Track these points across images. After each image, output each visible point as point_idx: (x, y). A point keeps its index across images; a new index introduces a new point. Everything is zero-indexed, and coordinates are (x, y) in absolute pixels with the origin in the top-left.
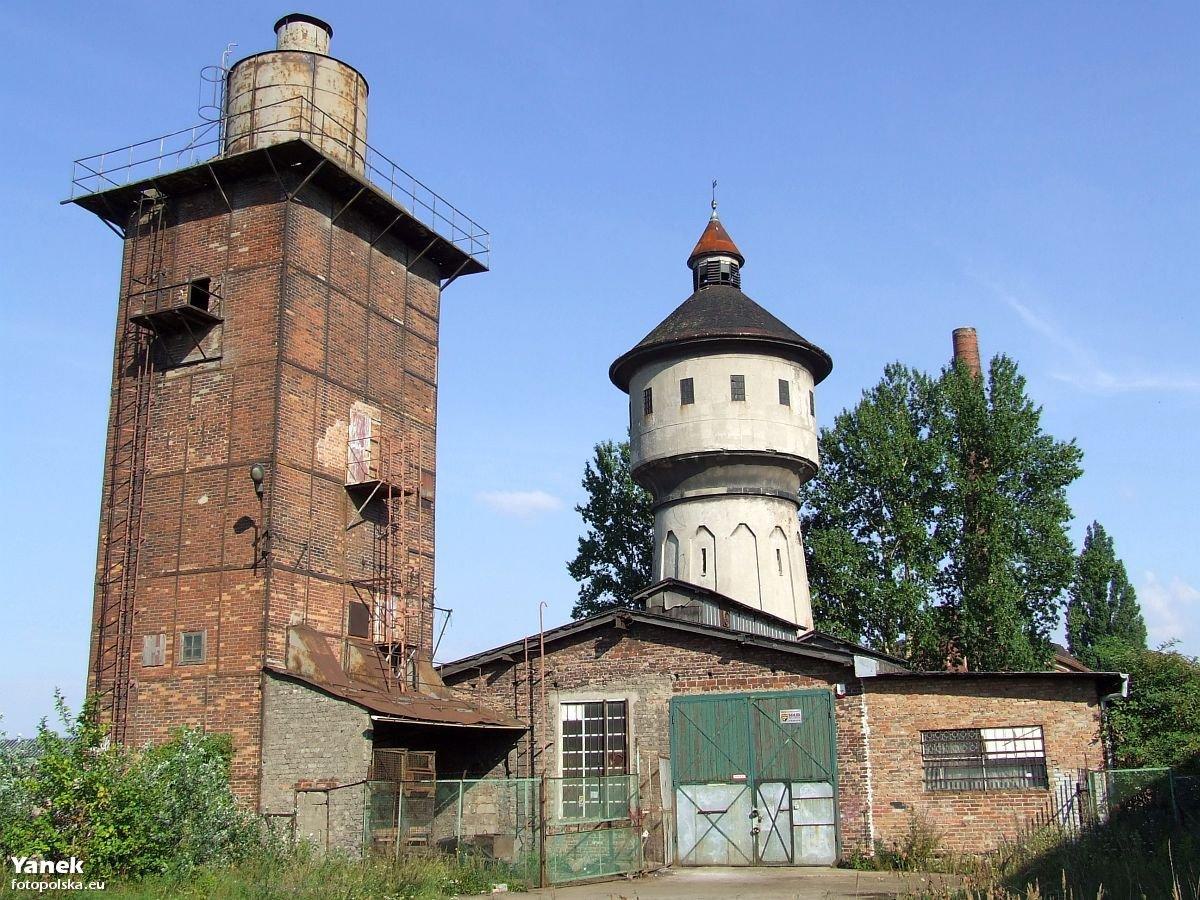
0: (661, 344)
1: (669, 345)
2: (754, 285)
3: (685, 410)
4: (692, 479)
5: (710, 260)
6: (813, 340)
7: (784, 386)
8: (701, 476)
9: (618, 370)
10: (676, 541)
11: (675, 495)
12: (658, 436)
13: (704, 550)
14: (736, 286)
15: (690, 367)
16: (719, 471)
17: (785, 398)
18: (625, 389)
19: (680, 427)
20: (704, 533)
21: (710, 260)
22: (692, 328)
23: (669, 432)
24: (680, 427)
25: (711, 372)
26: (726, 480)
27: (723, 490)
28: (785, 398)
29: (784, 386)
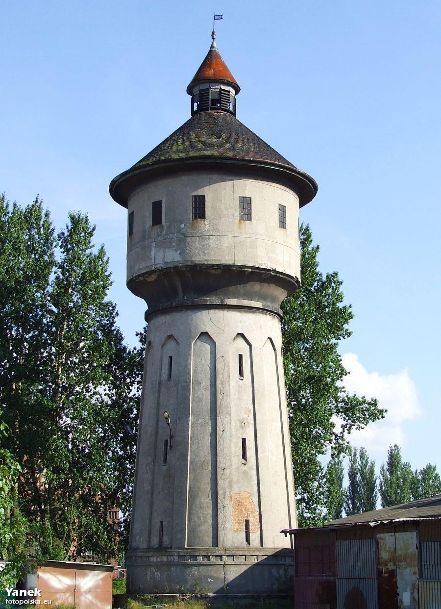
0: (235, 159)
1: (213, 161)
2: (253, 113)
3: (243, 225)
4: (232, 288)
5: (223, 87)
6: (301, 167)
7: (282, 210)
8: (241, 288)
9: (118, 185)
10: (213, 343)
11: (201, 300)
12: (213, 242)
13: (171, 358)
14: (234, 114)
15: (250, 187)
16: (257, 287)
17: (283, 223)
18: (124, 204)
19: (239, 239)
20: (241, 341)
21: (223, 87)
22: (176, 154)
23: (226, 242)
24: (239, 239)
25: (222, 195)
26: (262, 297)
27: (259, 304)
28: (283, 223)
29: (282, 210)
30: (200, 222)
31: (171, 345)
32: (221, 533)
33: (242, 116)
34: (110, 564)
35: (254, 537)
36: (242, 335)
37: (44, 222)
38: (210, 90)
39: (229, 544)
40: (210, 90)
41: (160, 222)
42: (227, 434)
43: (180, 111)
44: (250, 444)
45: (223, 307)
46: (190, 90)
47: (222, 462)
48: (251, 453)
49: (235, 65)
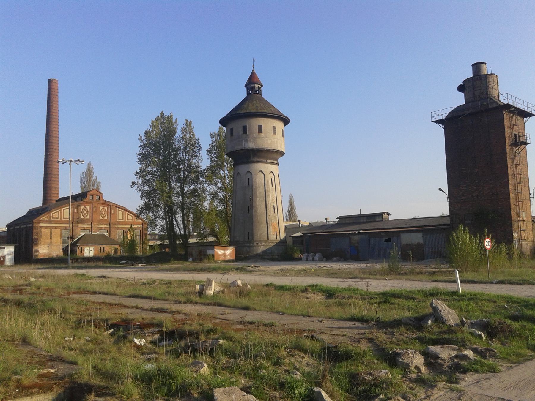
2: (269, 94)
20: (271, 174)
30: (261, 134)
31: (249, 174)
32: (269, 236)
33: (264, 95)
34: (490, 263)
35: (278, 237)
36: (261, 171)
37: (183, 130)
38: (252, 85)
39: (272, 239)
40: (252, 85)
41: (246, 133)
42: (269, 204)
43: (243, 94)
44: (276, 207)
45: (266, 162)
46: (246, 86)
47: (269, 213)
48: (276, 210)
49: (260, 76)
